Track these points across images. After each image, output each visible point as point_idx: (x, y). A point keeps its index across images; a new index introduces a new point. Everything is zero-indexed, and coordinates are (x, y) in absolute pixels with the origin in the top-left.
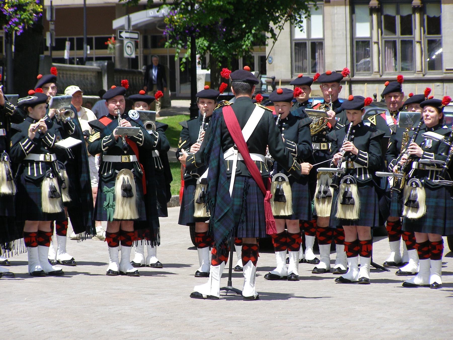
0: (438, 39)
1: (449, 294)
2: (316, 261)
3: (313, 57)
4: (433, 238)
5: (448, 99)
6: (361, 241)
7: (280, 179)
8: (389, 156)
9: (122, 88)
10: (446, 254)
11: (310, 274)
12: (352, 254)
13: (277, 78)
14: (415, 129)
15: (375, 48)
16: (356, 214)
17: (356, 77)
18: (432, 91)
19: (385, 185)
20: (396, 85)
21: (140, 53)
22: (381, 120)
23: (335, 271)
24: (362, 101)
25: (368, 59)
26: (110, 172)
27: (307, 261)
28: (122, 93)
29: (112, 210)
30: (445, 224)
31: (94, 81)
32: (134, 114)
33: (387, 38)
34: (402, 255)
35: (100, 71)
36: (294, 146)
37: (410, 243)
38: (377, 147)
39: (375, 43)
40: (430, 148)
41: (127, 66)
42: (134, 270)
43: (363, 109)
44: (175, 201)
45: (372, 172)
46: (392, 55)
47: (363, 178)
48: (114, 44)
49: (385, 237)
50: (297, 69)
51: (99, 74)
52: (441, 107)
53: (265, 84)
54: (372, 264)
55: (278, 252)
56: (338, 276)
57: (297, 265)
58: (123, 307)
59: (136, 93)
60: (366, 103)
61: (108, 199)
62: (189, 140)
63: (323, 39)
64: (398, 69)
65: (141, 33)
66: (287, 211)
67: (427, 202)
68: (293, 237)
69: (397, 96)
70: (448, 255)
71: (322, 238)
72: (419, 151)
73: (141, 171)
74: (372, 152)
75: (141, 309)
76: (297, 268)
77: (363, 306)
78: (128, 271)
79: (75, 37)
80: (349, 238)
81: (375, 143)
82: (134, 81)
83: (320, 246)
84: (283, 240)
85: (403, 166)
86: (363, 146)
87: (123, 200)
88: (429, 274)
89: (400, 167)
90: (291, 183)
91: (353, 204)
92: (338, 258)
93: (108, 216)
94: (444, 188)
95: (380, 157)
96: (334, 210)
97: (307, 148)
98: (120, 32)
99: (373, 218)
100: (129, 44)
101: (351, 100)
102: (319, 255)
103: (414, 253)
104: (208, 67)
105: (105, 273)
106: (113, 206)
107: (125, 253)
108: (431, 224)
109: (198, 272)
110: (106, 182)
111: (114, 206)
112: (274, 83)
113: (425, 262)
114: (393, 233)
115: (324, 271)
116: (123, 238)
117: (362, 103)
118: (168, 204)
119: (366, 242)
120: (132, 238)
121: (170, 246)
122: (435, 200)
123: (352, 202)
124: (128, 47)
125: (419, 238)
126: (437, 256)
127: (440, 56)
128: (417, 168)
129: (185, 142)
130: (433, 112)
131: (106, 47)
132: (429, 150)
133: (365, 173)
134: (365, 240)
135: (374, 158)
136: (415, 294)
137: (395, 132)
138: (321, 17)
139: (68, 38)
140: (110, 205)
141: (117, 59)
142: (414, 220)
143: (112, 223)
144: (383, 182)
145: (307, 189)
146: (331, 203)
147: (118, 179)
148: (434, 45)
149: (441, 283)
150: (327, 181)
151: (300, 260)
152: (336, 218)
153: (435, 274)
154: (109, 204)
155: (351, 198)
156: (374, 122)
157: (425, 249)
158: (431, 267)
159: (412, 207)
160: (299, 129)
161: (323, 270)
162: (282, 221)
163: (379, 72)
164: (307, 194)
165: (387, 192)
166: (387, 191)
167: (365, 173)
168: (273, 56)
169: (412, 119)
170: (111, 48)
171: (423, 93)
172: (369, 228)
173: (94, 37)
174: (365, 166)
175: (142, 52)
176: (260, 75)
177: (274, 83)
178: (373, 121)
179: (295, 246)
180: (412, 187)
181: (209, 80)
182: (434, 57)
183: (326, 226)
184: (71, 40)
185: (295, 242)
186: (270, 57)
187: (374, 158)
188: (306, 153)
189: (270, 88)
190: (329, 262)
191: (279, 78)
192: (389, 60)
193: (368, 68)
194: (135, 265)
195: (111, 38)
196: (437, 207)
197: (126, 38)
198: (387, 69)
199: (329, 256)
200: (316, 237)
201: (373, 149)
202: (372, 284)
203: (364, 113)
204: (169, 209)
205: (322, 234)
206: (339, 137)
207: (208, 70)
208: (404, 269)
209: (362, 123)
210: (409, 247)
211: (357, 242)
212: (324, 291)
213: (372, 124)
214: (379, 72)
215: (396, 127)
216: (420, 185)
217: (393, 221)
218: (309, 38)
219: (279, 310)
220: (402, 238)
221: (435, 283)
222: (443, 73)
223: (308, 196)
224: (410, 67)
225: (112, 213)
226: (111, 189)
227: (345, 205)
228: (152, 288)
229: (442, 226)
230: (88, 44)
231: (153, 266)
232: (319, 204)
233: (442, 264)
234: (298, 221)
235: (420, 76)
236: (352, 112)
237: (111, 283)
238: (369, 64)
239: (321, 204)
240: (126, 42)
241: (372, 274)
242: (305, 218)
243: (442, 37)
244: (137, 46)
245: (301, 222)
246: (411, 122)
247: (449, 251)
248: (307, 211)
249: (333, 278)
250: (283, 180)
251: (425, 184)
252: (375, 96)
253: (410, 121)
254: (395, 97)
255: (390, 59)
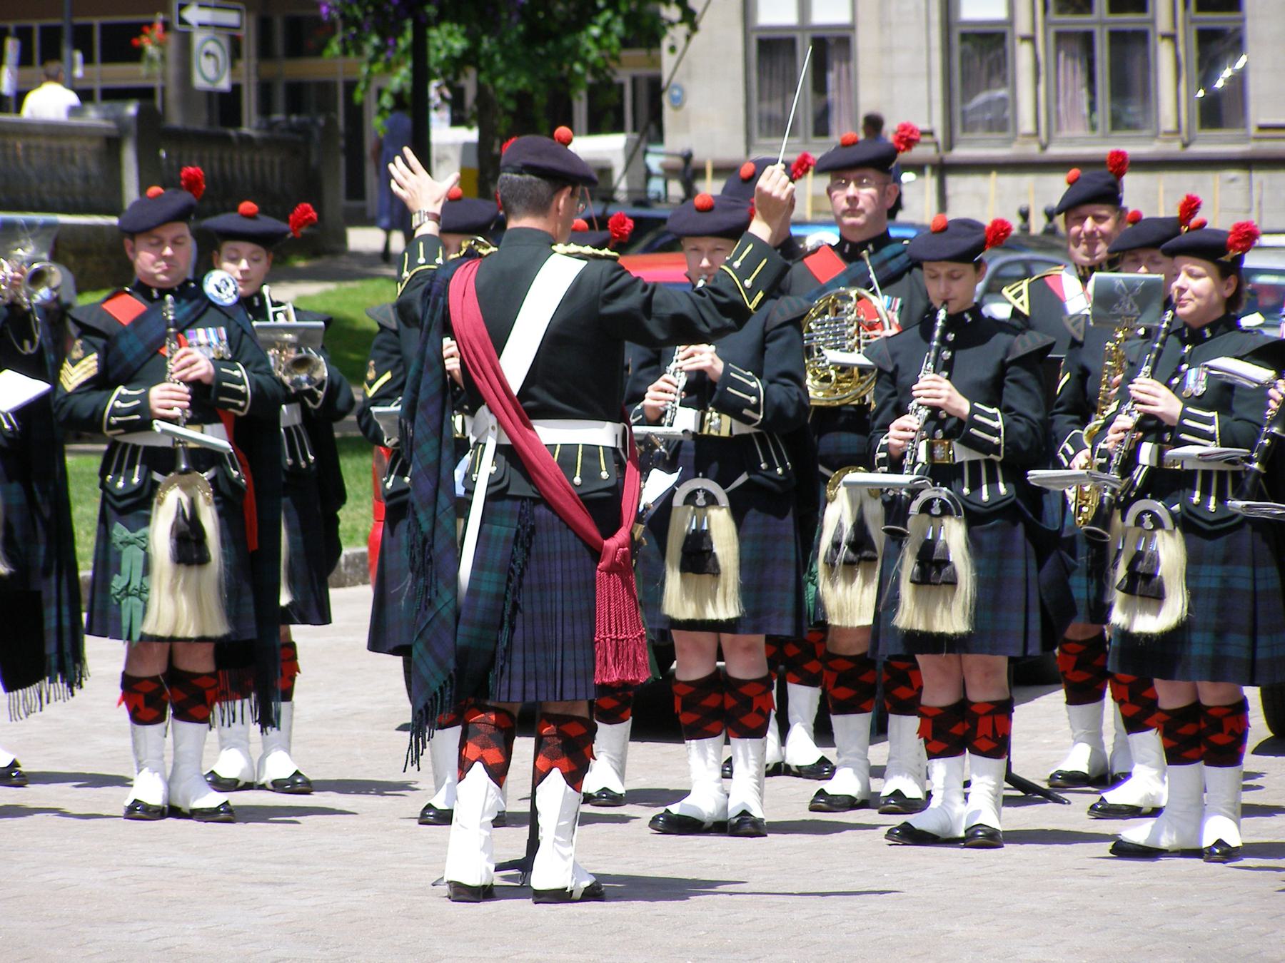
0: (1230, 26)
1: (1273, 879)
2: (822, 770)
3: (819, 85)
4: (1212, 695)
5: (1246, 233)
6: (974, 703)
7: (701, 500)
8: (1062, 421)
9: (184, 198)
10: (1256, 745)
11: (803, 813)
12: (945, 746)
13: (698, 157)
14: (1148, 334)
15: (1023, 57)
16: (961, 615)
17: (962, 152)
18: (1202, 206)
19: (1058, 515)
20: (1101, 178)
21: (249, 75)
22: (1046, 297)
23: (886, 803)
24: (977, 234)
25: (1002, 93)
26: (136, 480)
27: (794, 769)
28: (182, 215)
29: (137, 606)
30: (1254, 648)
31: (94, 168)
32: (222, 286)
33: (1064, 23)
34: (1109, 750)
35: (115, 133)
36: (753, 385)
37: (1134, 709)
38: (1029, 390)
39: (1024, 39)
40: (1199, 397)
41: (204, 116)
42: (213, 799)
43: (980, 261)
44: (357, 566)
45: (1016, 472)
46: (1081, 78)
47: (985, 497)
48: (160, 45)
49: (1051, 687)
50: (765, 126)
51: (112, 145)
52: (1226, 259)
53: (658, 176)
54: (1011, 779)
55: (693, 741)
56: (897, 820)
57: (760, 785)
58: (177, 926)
59: (225, 210)
60: (991, 237)
61: (125, 567)
62: (401, 369)
63: (852, 27)
64: (1100, 125)
65: (248, 10)
66: (725, 607)
67: (1191, 577)
68: (743, 690)
69: (1104, 219)
70: (1262, 749)
71: (844, 693)
72: (1167, 404)
73: (239, 477)
74: (1013, 404)
75: (237, 933)
76: (761, 794)
77: (977, 924)
78: (197, 805)
79: (36, 24)
80: (937, 695)
81: (1023, 374)
82: (227, 166)
83: (837, 721)
84: (712, 701)
85: (1116, 456)
86: (981, 385)
87: (175, 576)
88: (1200, 812)
89: (1104, 460)
90: (738, 514)
91: (953, 582)
92: (893, 762)
93: (125, 623)
94: (1248, 528)
95: (1041, 421)
96: (887, 604)
97: (796, 398)
98: (182, 7)
99: (1021, 627)
100: (211, 46)
101: (943, 230)
102: (834, 750)
103: (1149, 743)
104: (473, 117)
105: (122, 812)
106: (142, 592)
107: (187, 746)
108: (1208, 652)
109: (429, 807)
110: (122, 512)
111: (147, 591)
112: (688, 171)
113: (1188, 773)
114: (1081, 676)
115: (851, 803)
116: (182, 696)
117: (981, 236)
118: (332, 578)
119: (991, 707)
120: (210, 694)
121: (337, 719)
122: (1218, 571)
123: (949, 575)
124: (208, 54)
125: (1169, 695)
126: (1228, 755)
127: (1239, 80)
128: (1154, 464)
129: (388, 376)
130: (1198, 277)
131: (136, 55)
132: (1198, 401)
133: (992, 481)
134: (987, 700)
135: (1021, 427)
136: (1151, 882)
137: (1080, 338)
138: (199, 82)
139: (11, 25)
140: (131, 587)
141: (172, 93)
142: (1148, 638)
143: (141, 646)
144: (1051, 506)
145: (791, 532)
146: (877, 573)
147: (160, 503)
148: (1216, 47)
149: (1240, 844)
150: (861, 506)
151: (770, 768)
152: (895, 628)
153: (1220, 813)
154: (129, 584)
155: (947, 562)
156: (1022, 303)
157: (1188, 729)
158: (1205, 792)
159: (1142, 596)
160: (765, 334)
161: (846, 800)
162: (707, 638)
163: (1037, 133)
164: (788, 549)
165: (1067, 539)
166: (1064, 535)
167: (992, 481)
168: (685, 84)
169: (1136, 298)
170: (151, 60)
171: (1176, 213)
172: (1002, 662)
173: (96, 22)
174: (992, 456)
175: (253, 70)
176: (642, 146)
177: (689, 174)
178: (1020, 299)
179: (751, 720)
180: (1139, 529)
181: (474, 163)
182: (1219, 84)
183: (857, 652)
184: (24, 35)
185: (751, 708)
186: (676, 87)
187: (1021, 427)
188: (791, 412)
189: (676, 189)
190: (866, 772)
191: (706, 154)
192: (1070, 94)
193: (1001, 122)
194: (219, 784)
195: (151, 25)
196: (1226, 592)
197: (202, 25)
198: (1064, 123)
199: (866, 752)
200: (824, 691)
201: (1012, 394)
202: (1009, 848)
203: (983, 274)
204: (335, 594)
205: (842, 680)
206: (899, 360)
207: (470, 127)
208: (1115, 796)
209: (976, 310)
210: (1133, 724)
211: (962, 708)
212: (848, 870)
213: (1016, 312)
214: (1037, 133)
215: (1083, 321)
216: (1168, 522)
217: (1080, 638)
218: (804, 25)
219: (700, 937)
220: (1108, 693)
221: (1220, 843)
222: (1246, 139)
223: (793, 557)
224: (1140, 119)
225: (138, 614)
226: (139, 534)
227: (928, 586)
228: (275, 863)
229: (1245, 655)
230: (76, 46)
231: (278, 786)
232: (833, 584)
233: (1245, 779)
234: (760, 639)
235: (1173, 148)
236: (943, 269)
237: (138, 845)
238: (1005, 109)
239: (840, 587)
240: (198, 38)
241: (1008, 811)
242: (785, 628)
243: (1243, 20)
244: (235, 51)
245: (770, 640)
246: (1132, 307)
247: (1268, 734)
248: (789, 605)
249: (874, 827)
250: (712, 500)
251: (1183, 518)
252: (1025, 215)
253: (1128, 306)
254: (1098, 219)
255: (1075, 92)
